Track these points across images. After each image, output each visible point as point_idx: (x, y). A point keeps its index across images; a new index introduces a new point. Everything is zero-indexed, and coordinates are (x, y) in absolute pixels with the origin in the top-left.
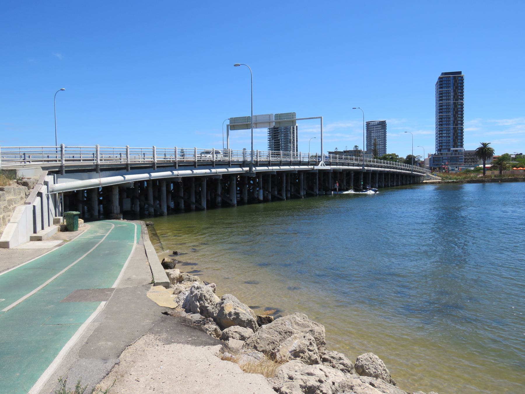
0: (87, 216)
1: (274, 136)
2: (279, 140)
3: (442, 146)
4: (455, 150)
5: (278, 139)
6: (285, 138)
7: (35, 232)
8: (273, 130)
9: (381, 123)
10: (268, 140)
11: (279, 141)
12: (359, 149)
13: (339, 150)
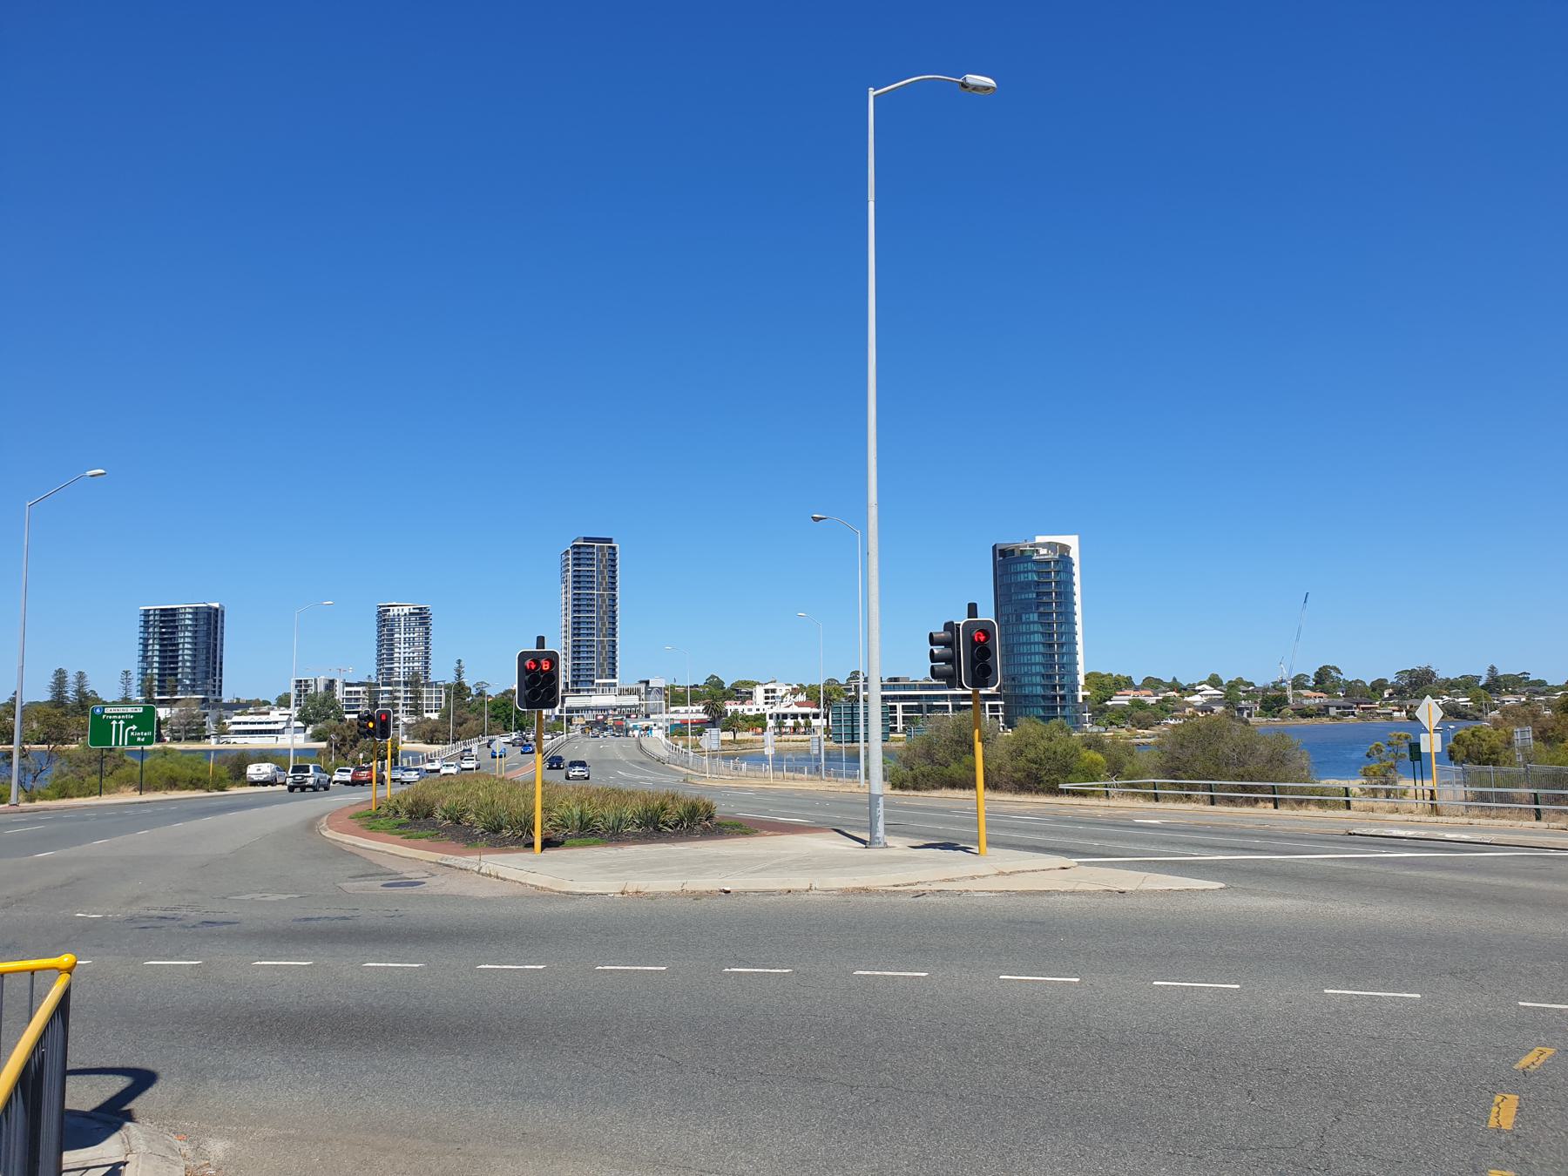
3: (579, 676)
9: (417, 611)
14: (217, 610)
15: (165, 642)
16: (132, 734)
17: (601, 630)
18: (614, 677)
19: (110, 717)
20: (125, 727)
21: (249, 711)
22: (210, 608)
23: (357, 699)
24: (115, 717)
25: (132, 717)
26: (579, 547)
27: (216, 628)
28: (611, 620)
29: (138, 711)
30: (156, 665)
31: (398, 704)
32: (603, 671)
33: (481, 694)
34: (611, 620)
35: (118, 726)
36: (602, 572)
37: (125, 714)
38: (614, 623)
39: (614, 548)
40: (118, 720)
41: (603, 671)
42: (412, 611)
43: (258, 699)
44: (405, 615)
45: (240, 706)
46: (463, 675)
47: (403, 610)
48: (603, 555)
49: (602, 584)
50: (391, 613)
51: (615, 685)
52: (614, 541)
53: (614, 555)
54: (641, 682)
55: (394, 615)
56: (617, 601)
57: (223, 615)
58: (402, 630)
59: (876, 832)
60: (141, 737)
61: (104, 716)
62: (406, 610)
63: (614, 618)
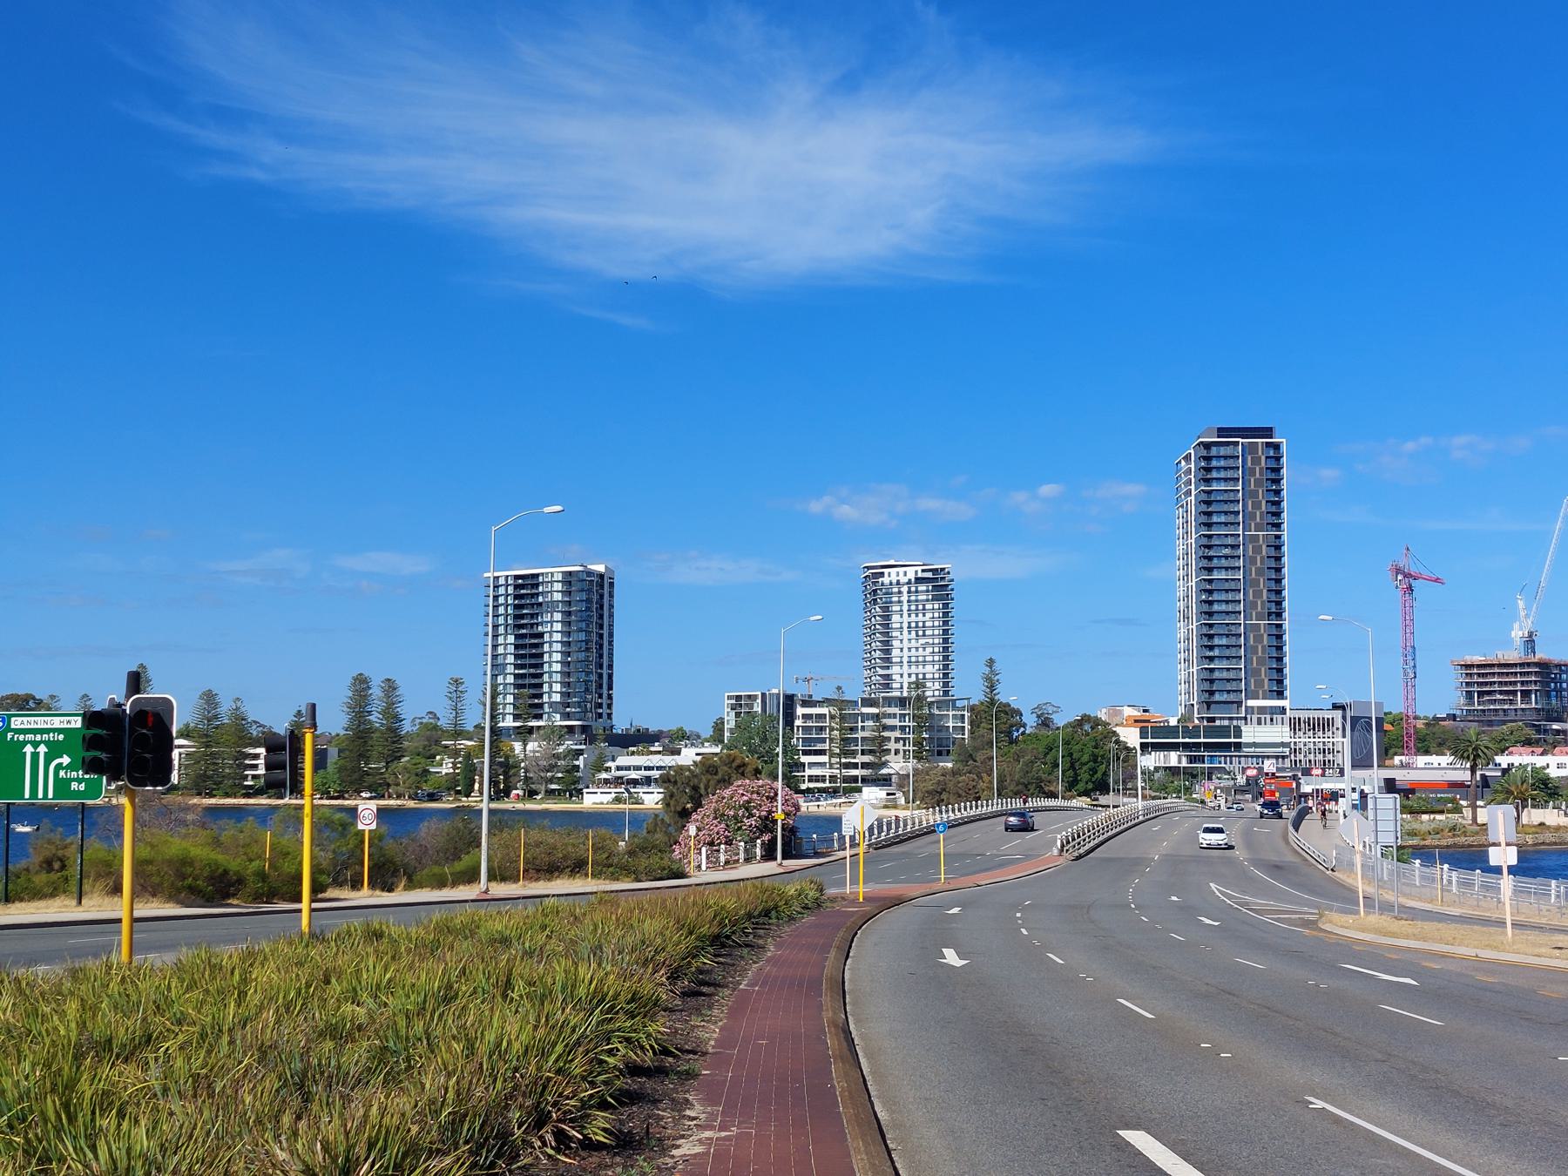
2: (541, 635)
7: (1282, 718)
9: (930, 575)
14: (601, 576)
15: (524, 631)
16: (62, 773)
18: (1280, 694)
19: (21, 738)
20: (49, 759)
21: (652, 749)
22: (590, 573)
23: (821, 729)
24: (30, 737)
25: (61, 737)
26: (1207, 446)
27: (602, 607)
28: (1273, 586)
29: (73, 725)
30: (510, 669)
31: (889, 739)
32: (1259, 684)
33: (1045, 723)
34: (1273, 586)
35: (35, 756)
36: (1254, 494)
37: (47, 731)
38: (1279, 592)
39: (1277, 447)
40: (36, 744)
41: (1259, 684)
42: (920, 575)
43: (681, 729)
44: (909, 582)
45: (638, 739)
46: (999, 688)
48: (1256, 461)
49: (1253, 516)
50: (886, 580)
51: (1283, 710)
52: (1276, 432)
53: (1278, 459)
54: (1335, 707)
55: (891, 584)
56: (1285, 549)
57: (611, 585)
58: (905, 608)
59: (1218, 572)
60: (79, 781)
61: (9, 735)
62: (911, 574)
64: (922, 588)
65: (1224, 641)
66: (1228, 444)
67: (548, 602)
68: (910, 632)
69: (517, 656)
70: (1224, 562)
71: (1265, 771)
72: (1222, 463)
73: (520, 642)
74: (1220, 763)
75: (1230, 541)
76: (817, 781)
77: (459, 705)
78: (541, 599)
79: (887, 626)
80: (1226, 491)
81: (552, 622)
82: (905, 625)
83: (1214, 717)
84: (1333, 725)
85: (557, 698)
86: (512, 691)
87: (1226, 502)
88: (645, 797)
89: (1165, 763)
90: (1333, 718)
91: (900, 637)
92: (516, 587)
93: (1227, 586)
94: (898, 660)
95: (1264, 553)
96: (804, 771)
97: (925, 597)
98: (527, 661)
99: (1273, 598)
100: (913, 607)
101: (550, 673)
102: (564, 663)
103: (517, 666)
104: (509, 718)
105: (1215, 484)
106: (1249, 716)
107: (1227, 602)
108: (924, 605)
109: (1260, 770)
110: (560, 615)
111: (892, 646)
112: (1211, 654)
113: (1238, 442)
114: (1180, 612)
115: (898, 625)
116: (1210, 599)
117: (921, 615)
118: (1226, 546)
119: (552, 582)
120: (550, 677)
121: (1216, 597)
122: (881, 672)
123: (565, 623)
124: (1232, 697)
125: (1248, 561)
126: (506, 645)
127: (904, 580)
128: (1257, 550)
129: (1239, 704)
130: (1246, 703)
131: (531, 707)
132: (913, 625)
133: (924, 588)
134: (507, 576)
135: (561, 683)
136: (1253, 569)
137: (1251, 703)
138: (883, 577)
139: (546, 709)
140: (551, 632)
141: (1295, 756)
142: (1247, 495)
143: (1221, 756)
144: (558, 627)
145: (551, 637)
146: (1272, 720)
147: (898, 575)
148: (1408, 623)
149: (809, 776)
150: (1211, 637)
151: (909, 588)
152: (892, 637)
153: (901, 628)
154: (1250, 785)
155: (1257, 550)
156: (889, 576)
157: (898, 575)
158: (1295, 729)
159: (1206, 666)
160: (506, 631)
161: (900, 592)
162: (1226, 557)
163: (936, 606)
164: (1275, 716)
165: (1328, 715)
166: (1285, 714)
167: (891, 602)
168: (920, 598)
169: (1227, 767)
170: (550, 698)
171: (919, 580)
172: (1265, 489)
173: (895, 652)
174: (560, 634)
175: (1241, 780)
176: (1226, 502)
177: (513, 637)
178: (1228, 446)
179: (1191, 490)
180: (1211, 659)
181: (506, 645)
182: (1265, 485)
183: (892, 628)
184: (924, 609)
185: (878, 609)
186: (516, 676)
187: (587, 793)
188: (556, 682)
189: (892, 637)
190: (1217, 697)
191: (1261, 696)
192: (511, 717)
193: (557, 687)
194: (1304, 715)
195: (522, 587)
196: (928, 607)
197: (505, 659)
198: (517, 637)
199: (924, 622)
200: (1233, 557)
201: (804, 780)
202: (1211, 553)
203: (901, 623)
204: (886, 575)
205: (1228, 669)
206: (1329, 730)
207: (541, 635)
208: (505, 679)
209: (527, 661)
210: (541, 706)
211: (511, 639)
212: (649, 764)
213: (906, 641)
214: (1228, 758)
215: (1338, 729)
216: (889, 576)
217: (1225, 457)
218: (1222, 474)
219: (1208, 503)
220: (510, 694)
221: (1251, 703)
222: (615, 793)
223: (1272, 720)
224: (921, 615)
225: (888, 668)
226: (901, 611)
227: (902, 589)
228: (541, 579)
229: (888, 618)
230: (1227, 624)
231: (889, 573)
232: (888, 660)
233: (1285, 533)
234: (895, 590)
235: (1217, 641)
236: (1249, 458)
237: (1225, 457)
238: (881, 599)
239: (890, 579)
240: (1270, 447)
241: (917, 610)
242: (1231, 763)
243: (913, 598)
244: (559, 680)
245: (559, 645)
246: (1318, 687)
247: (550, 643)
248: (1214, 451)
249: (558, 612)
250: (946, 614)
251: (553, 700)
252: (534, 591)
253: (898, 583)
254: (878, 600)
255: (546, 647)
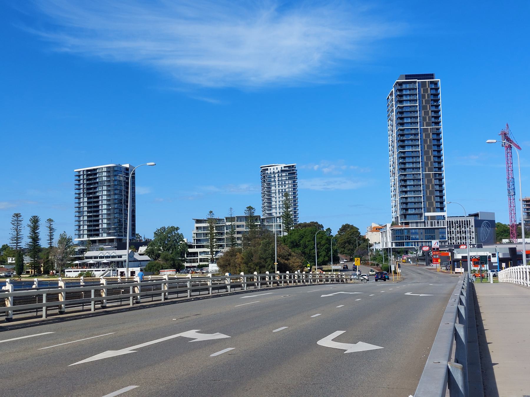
0: (363, 245)
1: (88, 189)
2: (98, 197)
4: (431, 216)
5: (98, 194)
6: (109, 212)
7: (444, 221)
8: (85, 173)
9: (287, 169)
10: (76, 198)
11: (97, 218)
12: (256, 214)
13: (216, 217)
14: (127, 169)
15: (91, 196)
17: (427, 164)
18: (442, 209)
26: (400, 84)
28: (436, 154)
30: (86, 214)
32: (431, 204)
34: (436, 154)
39: (436, 83)
41: (431, 204)
42: (283, 169)
44: (278, 172)
47: (277, 168)
48: (426, 91)
50: (269, 172)
52: (435, 76)
53: (437, 89)
54: (470, 215)
55: (271, 173)
58: (277, 183)
63: (439, 151)
64: (284, 174)
65: (412, 183)
66: (411, 82)
67: (101, 181)
68: (279, 194)
69: (88, 207)
70: (410, 143)
71: (433, 247)
72: (408, 92)
73: (90, 200)
74: (412, 245)
75: (413, 132)
76: (204, 261)
77: (19, 227)
78: (98, 180)
79: (269, 192)
80: (410, 106)
81: (102, 191)
82: (277, 191)
83: (408, 222)
84: (470, 225)
85: (105, 226)
86: (86, 224)
87: (411, 112)
88: (96, 273)
89: (386, 247)
90: (469, 221)
91: (275, 196)
92: (88, 175)
93: (413, 155)
94: (275, 206)
95: (431, 137)
96: (198, 256)
97: (285, 178)
98: (92, 209)
99: (436, 160)
100: (280, 183)
101: (102, 214)
102: (108, 210)
103: (88, 212)
104: (86, 236)
105: (405, 103)
106: (426, 221)
107: (413, 163)
108: (285, 182)
109: (430, 247)
110: (106, 187)
111: (272, 200)
112: (405, 190)
113: (416, 81)
114: (391, 172)
115: (274, 191)
116: (404, 161)
117: (283, 186)
118: (412, 134)
119: (102, 172)
120: (102, 216)
121: (407, 160)
122: (268, 212)
123: (108, 191)
124: (417, 211)
125: (423, 142)
126: (83, 202)
127: (276, 171)
128: (428, 136)
129: (421, 215)
130: (424, 214)
131: (94, 230)
132: (281, 191)
133: (285, 174)
134: (84, 170)
135: (107, 219)
136: (426, 146)
137: (427, 214)
138: (268, 170)
139: (101, 232)
140: (102, 196)
141: (451, 241)
142: (421, 108)
143: (412, 242)
144: (105, 193)
145: (102, 198)
146: (438, 223)
147: (274, 169)
148: (510, 169)
149: (200, 259)
150: (405, 181)
151: (278, 175)
152: (272, 197)
153: (276, 192)
154: (424, 256)
155: (428, 136)
156: (270, 170)
157: (274, 169)
158: (450, 227)
159: (403, 196)
160: (84, 196)
161: (275, 177)
162: (412, 140)
163: (290, 182)
164: (439, 221)
165: (468, 219)
166: (445, 219)
167: (271, 181)
168: (283, 179)
169: (416, 247)
170: (102, 226)
171: (282, 171)
172: (430, 105)
173: (273, 203)
174: (106, 196)
175: (420, 253)
176: (411, 112)
177: (86, 198)
178: (411, 84)
179: (393, 109)
180: (406, 192)
181: (83, 202)
182: (431, 103)
183: (272, 193)
184: (285, 184)
185: (265, 185)
186: (88, 217)
187: (67, 272)
188: (105, 219)
189: (272, 197)
190: (410, 212)
191: (432, 211)
192: (86, 235)
193: (105, 221)
194: (454, 220)
195: (90, 175)
196: (286, 182)
197: (83, 209)
198: (88, 198)
199: (285, 189)
200: (415, 140)
201: (197, 261)
202: (404, 138)
203: (275, 190)
204: (269, 170)
205: (415, 197)
206: (468, 227)
207: (98, 197)
208: (83, 218)
209: (92, 209)
210: (98, 230)
211: (86, 200)
212: (114, 254)
213: (277, 198)
214: (416, 243)
215: (472, 226)
216: (270, 170)
217: (410, 89)
218: (408, 98)
219: (401, 113)
220: (86, 225)
221: (427, 214)
222: (81, 271)
223: (438, 223)
224: (283, 186)
225: (270, 210)
226: (275, 185)
227: (275, 175)
228: (98, 171)
229: (270, 188)
230: (413, 174)
231: (270, 169)
232: (270, 207)
233: (442, 127)
234: (273, 176)
235: (408, 183)
236: (422, 89)
237: (410, 89)
238: (267, 180)
239: (270, 171)
240: (432, 100)
241: (282, 184)
242: (418, 245)
243: (280, 179)
244: (106, 218)
245: (106, 201)
246: (488, 141)
247: (102, 200)
248: (404, 86)
249: (105, 186)
250: (294, 185)
251: (104, 227)
252: (95, 177)
253: (274, 172)
254: (266, 181)
255: (100, 203)
